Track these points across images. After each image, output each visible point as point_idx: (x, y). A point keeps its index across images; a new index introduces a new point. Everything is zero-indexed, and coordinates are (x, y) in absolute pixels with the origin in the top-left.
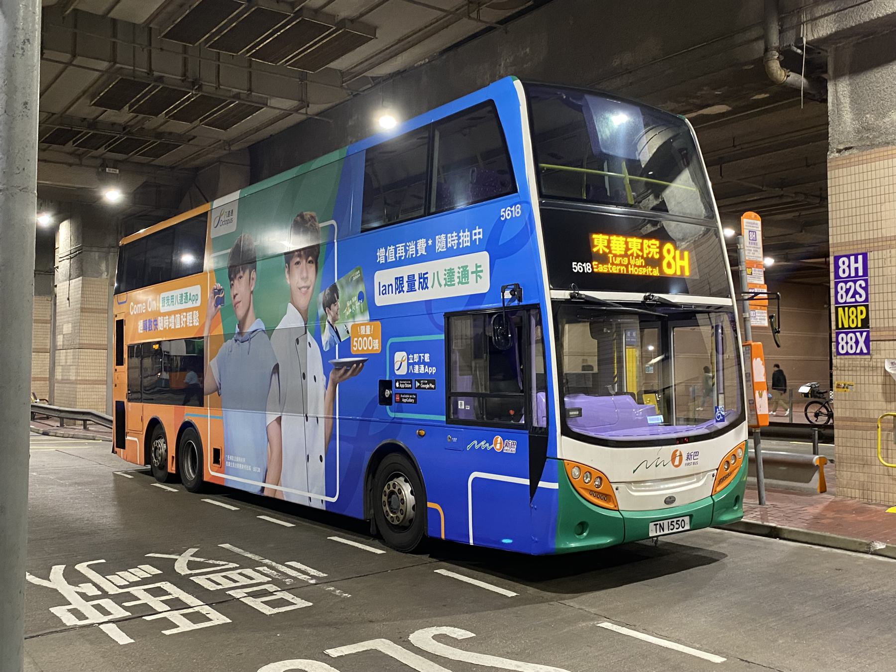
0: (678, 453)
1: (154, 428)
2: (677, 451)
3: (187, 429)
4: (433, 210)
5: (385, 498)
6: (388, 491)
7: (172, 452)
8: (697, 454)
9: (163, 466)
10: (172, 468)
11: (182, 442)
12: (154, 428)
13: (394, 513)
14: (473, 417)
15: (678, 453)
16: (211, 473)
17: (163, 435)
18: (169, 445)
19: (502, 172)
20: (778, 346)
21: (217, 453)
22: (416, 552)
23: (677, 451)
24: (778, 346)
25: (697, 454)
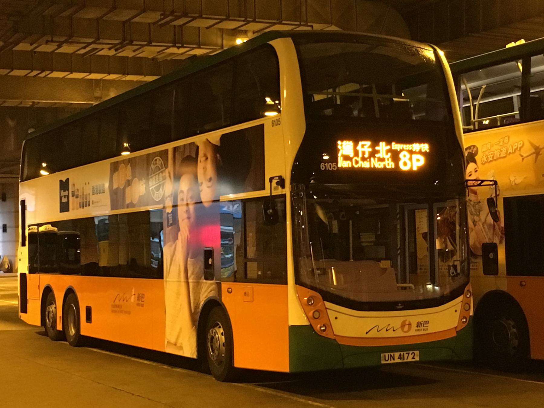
2: (406, 320)
7: (59, 314)
8: (427, 322)
16: (86, 330)
21: (89, 311)
25: (427, 322)
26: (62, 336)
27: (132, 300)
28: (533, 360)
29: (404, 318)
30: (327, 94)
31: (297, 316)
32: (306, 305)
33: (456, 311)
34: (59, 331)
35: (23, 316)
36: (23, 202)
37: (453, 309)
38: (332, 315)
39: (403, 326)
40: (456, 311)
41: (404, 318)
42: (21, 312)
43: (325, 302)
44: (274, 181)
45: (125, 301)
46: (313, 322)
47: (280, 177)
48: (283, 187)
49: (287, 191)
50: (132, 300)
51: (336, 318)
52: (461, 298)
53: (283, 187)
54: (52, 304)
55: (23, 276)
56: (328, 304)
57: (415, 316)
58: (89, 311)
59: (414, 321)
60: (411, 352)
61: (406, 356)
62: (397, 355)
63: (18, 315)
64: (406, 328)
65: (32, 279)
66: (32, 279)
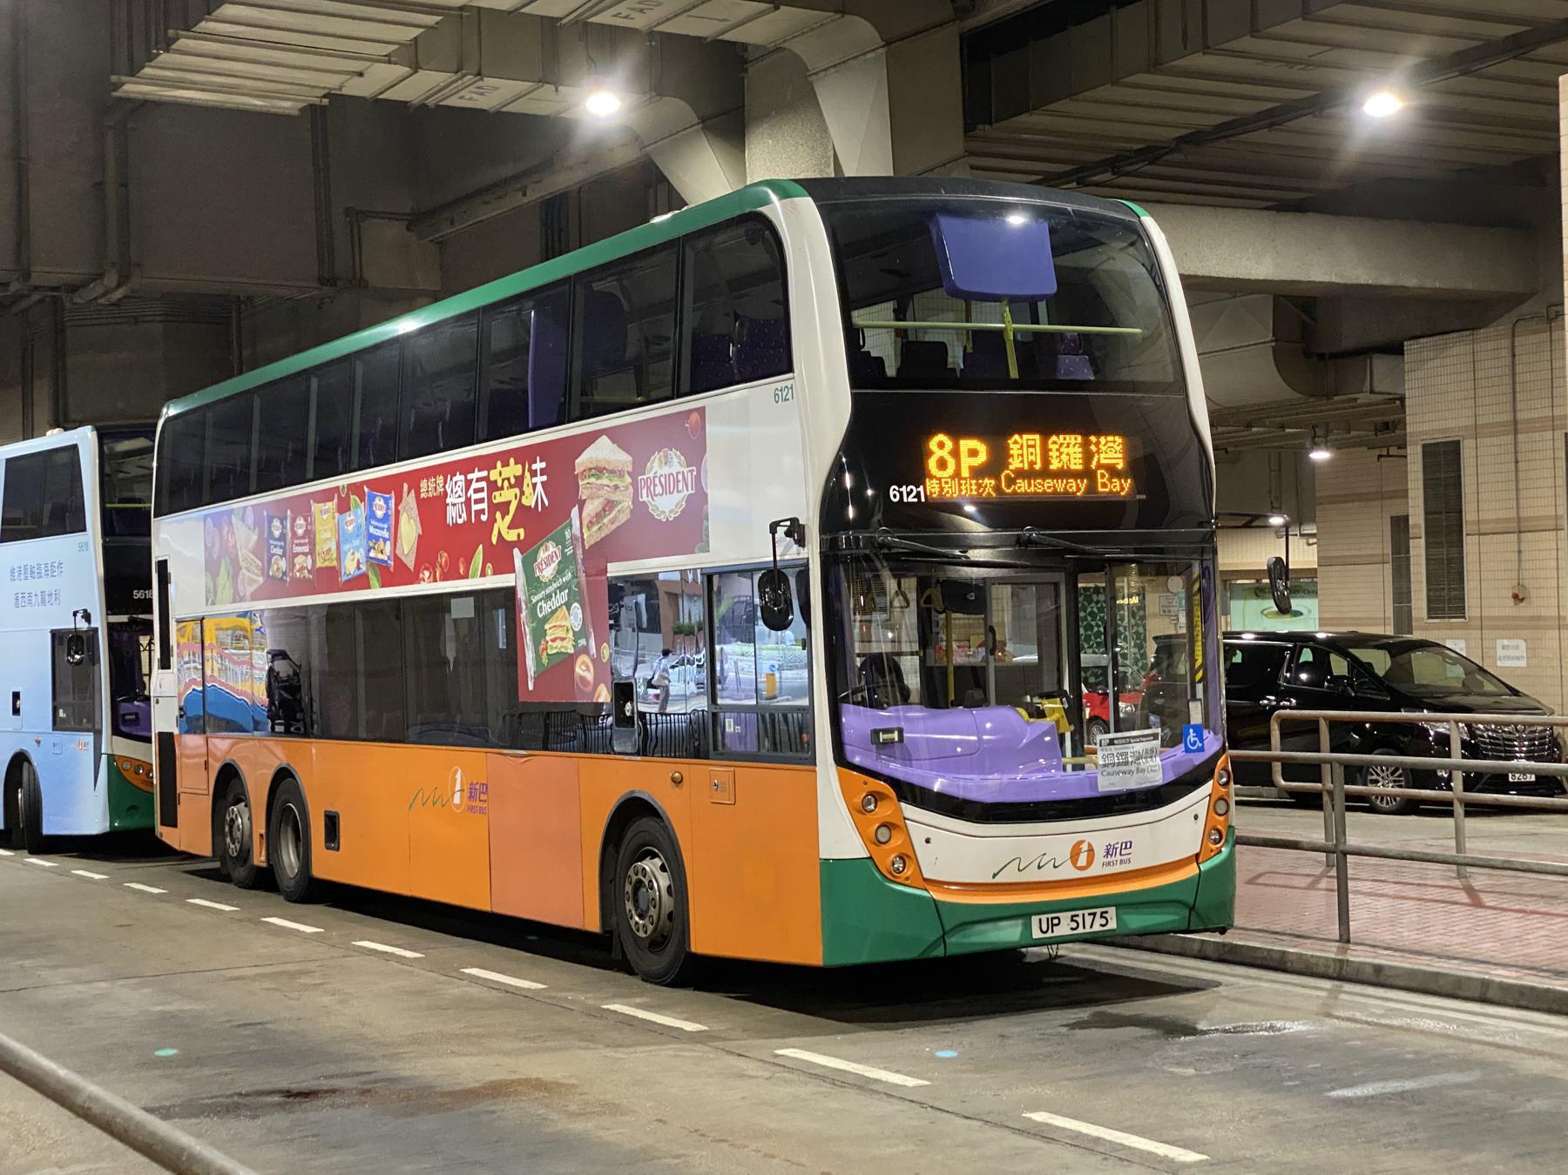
0: (1085, 847)
1: (228, 782)
2: (1082, 842)
3: (283, 776)
4: (685, 386)
5: (629, 888)
6: (634, 878)
7: (260, 828)
8: (1128, 845)
9: (245, 854)
10: (259, 858)
11: (277, 805)
12: (228, 782)
13: (641, 917)
14: (752, 747)
15: (1085, 847)
16: (327, 865)
17: (241, 798)
18: (251, 818)
19: (777, 302)
20: (16, 711)
21: (332, 822)
22: (675, 984)
23: (1082, 842)
24: (16, 711)
25: (1128, 845)
26: (265, 881)
27: (457, 800)
28: (695, 955)
29: (1078, 837)
30: (979, 731)
31: (840, 836)
32: (859, 811)
33: (1196, 817)
34: (259, 868)
35: (166, 834)
36: (163, 565)
37: (1191, 813)
38: (917, 833)
39: (1074, 856)
40: (1196, 817)
41: (1078, 837)
42: (163, 824)
43: (903, 805)
44: (781, 531)
45: (439, 804)
46: (878, 853)
47: (794, 521)
48: (801, 542)
49: (812, 553)
50: (457, 800)
51: (928, 841)
52: (1207, 788)
53: (801, 542)
54: (237, 801)
55: (167, 740)
56: (909, 810)
57: (1099, 832)
58: (332, 822)
59: (1099, 842)
60: (1098, 911)
61: (1089, 919)
62: (1065, 917)
63: (153, 829)
64: (1082, 860)
65: (191, 743)
66: (191, 743)
